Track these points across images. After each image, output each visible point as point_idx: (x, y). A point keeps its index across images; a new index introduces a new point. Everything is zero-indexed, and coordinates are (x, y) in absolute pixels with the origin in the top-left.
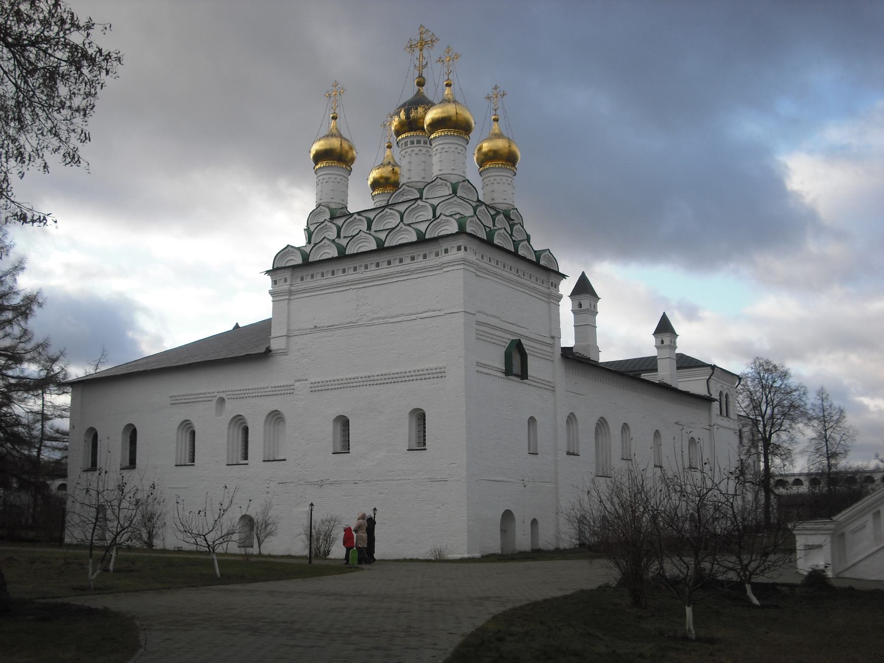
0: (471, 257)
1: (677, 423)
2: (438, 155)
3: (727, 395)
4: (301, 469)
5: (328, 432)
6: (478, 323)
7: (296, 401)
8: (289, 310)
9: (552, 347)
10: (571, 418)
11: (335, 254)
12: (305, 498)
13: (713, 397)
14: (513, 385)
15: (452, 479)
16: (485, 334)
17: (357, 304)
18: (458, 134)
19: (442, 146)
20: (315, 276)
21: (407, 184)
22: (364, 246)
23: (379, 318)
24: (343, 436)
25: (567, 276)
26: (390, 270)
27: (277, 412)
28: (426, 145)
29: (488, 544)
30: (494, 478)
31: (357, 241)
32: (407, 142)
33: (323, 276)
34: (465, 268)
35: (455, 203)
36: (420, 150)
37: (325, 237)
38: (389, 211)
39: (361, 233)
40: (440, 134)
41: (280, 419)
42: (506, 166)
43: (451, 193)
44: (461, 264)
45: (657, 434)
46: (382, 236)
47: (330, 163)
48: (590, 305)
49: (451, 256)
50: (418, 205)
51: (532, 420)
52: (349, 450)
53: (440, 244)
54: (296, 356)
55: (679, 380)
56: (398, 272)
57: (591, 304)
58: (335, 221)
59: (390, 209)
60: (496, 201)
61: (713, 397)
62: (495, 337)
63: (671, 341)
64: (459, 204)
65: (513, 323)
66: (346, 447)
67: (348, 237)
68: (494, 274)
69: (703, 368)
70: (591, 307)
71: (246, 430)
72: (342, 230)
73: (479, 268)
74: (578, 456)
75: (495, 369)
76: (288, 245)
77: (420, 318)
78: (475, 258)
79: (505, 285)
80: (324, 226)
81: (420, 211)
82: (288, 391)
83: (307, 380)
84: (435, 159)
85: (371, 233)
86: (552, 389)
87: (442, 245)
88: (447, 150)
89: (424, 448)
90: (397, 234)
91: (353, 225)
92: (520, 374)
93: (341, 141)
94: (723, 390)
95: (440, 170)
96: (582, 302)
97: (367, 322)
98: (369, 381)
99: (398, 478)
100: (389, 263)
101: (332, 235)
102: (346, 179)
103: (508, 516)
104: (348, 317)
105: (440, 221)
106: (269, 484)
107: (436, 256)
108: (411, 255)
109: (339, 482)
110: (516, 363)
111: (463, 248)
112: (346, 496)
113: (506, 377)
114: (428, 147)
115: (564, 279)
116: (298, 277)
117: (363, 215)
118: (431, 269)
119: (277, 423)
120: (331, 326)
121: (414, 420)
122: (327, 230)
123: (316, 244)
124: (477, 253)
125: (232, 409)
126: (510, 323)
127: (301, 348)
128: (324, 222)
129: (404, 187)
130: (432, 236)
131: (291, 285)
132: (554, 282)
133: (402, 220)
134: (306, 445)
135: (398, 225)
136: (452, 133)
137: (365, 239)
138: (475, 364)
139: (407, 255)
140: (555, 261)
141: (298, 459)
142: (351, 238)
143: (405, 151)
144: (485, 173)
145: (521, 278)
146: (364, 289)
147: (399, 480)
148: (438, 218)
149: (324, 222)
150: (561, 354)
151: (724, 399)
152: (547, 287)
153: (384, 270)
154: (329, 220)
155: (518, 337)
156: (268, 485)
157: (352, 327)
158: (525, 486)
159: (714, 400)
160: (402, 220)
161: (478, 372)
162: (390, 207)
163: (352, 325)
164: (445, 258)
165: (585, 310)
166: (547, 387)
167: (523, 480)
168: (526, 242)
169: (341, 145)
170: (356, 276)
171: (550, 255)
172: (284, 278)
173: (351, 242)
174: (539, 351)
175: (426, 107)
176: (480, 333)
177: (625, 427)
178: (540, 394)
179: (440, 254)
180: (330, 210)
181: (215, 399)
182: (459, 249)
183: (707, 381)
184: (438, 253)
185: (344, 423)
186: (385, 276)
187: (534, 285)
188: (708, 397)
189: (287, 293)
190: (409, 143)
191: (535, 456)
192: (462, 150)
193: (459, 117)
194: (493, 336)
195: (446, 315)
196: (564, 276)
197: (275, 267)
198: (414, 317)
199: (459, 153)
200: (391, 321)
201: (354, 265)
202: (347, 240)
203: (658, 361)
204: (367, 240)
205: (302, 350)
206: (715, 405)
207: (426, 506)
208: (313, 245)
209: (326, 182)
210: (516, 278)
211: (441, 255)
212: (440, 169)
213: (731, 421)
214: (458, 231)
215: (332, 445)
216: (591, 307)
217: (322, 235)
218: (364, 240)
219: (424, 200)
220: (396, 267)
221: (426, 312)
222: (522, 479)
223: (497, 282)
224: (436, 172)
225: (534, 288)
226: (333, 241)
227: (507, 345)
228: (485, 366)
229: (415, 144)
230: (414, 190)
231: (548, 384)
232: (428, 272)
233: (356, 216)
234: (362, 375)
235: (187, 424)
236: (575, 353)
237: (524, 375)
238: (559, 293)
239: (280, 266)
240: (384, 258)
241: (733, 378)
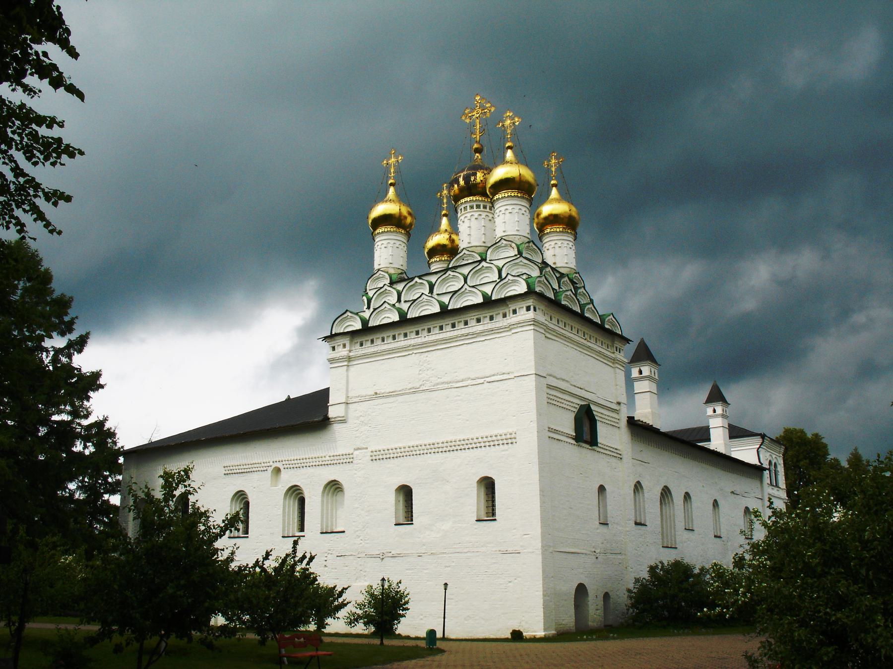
0: (542, 318)
1: (732, 492)
2: (502, 216)
3: (775, 463)
4: (361, 542)
5: (390, 502)
6: (549, 386)
7: (356, 470)
8: (348, 376)
9: (618, 413)
10: (638, 487)
11: (396, 318)
12: (365, 572)
13: (764, 466)
14: (584, 453)
15: (525, 550)
16: (556, 399)
17: (420, 369)
18: (522, 195)
19: (506, 207)
20: (375, 341)
21: (467, 249)
22: (427, 309)
23: (443, 383)
24: (406, 506)
25: (631, 341)
26: (455, 333)
27: (336, 483)
28: (486, 210)
29: (563, 620)
31: (418, 305)
32: (467, 207)
33: (383, 340)
34: (535, 329)
35: (521, 263)
36: (480, 215)
37: (385, 302)
38: (452, 274)
39: (424, 296)
40: (503, 196)
41: (338, 490)
42: (567, 230)
43: (517, 254)
44: (531, 325)
45: (716, 504)
46: (445, 299)
48: (651, 371)
49: (520, 317)
50: (483, 266)
51: (602, 489)
52: (412, 520)
53: (508, 305)
54: (355, 423)
55: (732, 449)
56: (463, 335)
58: (394, 286)
59: (453, 271)
60: (558, 265)
61: (763, 466)
62: (565, 402)
63: (723, 410)
64: (525, 265)
66: (409, 517)
67: (409, 301)
68: (562, 336)
69: (745, 438)
70: (651, 374)
71: (302, 502)
72: (403, 295)
73: (547, 329)
74: (645, 526)
75: (565, 435)
77: (487, 382)
78: (544, 319)
79: (573, 348)
80: (384, 291)
81: (485, 273)
82: (348, 460)
83: (367, 448)
84: (499, 220)
85: (433, 296)
86: (619, 456)
87: (510, 306)
88: (511, 211)
89: (493, 518)
90: (461, 296)
91: (415, 288)
92: (590, 441)
93: (400, 206)
94: (772, 460)
95: (504, 231)
96: (642, 368)
97: (430, 387)
98: (435, 449)
99: (466, 550)
100: (453, 326)
101: (393, 299)
103: (581, 590)
104: (410, 383)
105: (507, 282)
106: (326, 557)
107: (503, 317)
108: (477, 317)
109: (401, 555)
110: (586, 429)
111: (532, 308)
112: (409, 569)
114: (487, 212)
115: (628, 344)
116: (357, 342)
117: (424, 278)
118: (499, 331)
119: (335, 494)
120: (392, 392)
121: (483, 490)
122: (386, 295)
123: (375, 310)
124: (546, 315)
125: (288, 479)
126: (578, 387)
127: (361, 416)
128: (384, 286)
129: (464, 251)
130: (499, 298)
131: (350, 351)
132: (618, 347)
133: (466, 282)
134: (367, 516)
135: (462, 287)
136: (516, 194)
137: (427, 302)
138: (547, 429)
139: (472, 318)
140: (618, 325)
141: (358, 531)
142: (412, 302)
143: (464, 216)
144: (546, 237)
145: (588, 341)
146: (427, 354)
147: (466, 553)
148: (505, 278)
149: (384, 286)
150: (627, 421)
151: (772, 467)
153: (448, 333)
154: (389, 285)
155: (587, 402)
156: (326, 559)
157: (414, 392)
158: (597, 558)
159: (765, 469)
160: (466, 282)
161: (549, 437)
162: (452, 270)
163: (415, 391)
164: (512, 319)
165: (646, 377)
166: (615, 455)
167: (595, 552)
168: (591, 306)
169: (400, 210)
170: (419, 340)
172: (343, 344)
173: (413, 305)
174: (606, 417)
175: (486, 172)
176: (551, 397)
177: (687, 496)
178: (609, 462)
179: (507, 315)
180: (388, 275)
181: (270, 470)
182: (528, 309)
184: (506, 315)
185: (406, 492)
186: (449, 339)
187: (600, 349)
189: (346, 359)
190: (468, 207)
191: (605, 526)
193: (522, 179)
194: (563, 401)
195: (515, 378)
197: (333, 333)
198: (481, 381)
199: (523, 214)
200: (456, 386)
201: (417, 329)
202: (408, 304)
204: (430, 304)
205: (361, 417)
207: (497, 580)
208: (373, 310)
209: (385, 247)
210: (583, 341)
211: (509, 316)
212: (504, 230)
213: (781, 490)
214: (526, 290)
215: (394, 516)
216: (651, 374)
217: (381, 300)
218: (426, 303)
219: (488, 261)
220: (461, 330)
221: (494, 375)
222: (594, 550)
223: (565, 344)
224: (499, 233)
225: (600, 352)
226: (394, 305)
227: (576, 410)
228: (556, 432)
229: (475, 209)
230: (476, 255)
231: (615, 451)
232: (496, 334)
233: (417, 279)
234: (427, 442)
235: (335, 484)
236: (636, 420)
237: (593, 442)
239: (339, 332)
240: (447, 322)
241: (780, 448)
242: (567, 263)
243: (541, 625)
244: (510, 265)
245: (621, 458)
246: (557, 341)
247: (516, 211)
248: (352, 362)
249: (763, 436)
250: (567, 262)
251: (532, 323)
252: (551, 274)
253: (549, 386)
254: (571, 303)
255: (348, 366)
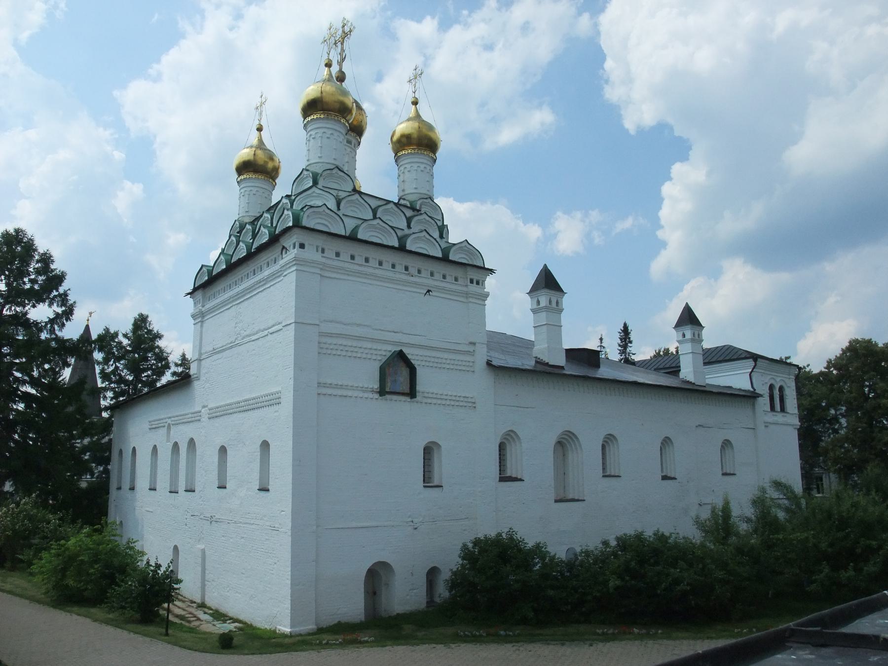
30: (354, 524)
32: (351, 144)
35: (314, 194)
47: (251, 175)
57: (552, 300)
60: (406, 192)
65: (396, 331)
76: (203, 266)
87: (468, 273)
92: (409, 392)
102: (269, 193)
113: (381, 398)
152: (465, 284)
157: (231, 347)
167: (412, 521)
169: (254, 154)
171: (468, 246)
183: (750, 375)
188: (752, 392)
189: (199, 316)
192: (425, 168)
196: (491, 271)
203: (681, 357)
206: (763, 403)
222: (410, 519)
238: (485, 290)
240: (401, 260)
242: (416, 188)
243: (288, 620)
244: (301, 198)
245: (475, 407)
246: (335, 278)
247: (319, 135)
248: (206, 316)
249: (755, 357)
250: (416, 187)
251: (294, 263)
252: (361, 202)
253: (321, 334)
254: (384, 234)
255: (321, 276)
